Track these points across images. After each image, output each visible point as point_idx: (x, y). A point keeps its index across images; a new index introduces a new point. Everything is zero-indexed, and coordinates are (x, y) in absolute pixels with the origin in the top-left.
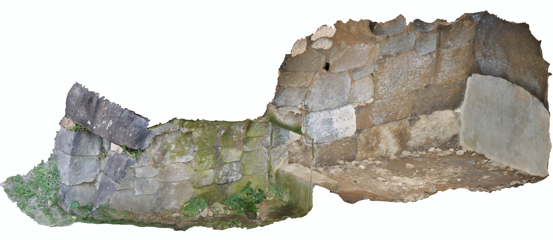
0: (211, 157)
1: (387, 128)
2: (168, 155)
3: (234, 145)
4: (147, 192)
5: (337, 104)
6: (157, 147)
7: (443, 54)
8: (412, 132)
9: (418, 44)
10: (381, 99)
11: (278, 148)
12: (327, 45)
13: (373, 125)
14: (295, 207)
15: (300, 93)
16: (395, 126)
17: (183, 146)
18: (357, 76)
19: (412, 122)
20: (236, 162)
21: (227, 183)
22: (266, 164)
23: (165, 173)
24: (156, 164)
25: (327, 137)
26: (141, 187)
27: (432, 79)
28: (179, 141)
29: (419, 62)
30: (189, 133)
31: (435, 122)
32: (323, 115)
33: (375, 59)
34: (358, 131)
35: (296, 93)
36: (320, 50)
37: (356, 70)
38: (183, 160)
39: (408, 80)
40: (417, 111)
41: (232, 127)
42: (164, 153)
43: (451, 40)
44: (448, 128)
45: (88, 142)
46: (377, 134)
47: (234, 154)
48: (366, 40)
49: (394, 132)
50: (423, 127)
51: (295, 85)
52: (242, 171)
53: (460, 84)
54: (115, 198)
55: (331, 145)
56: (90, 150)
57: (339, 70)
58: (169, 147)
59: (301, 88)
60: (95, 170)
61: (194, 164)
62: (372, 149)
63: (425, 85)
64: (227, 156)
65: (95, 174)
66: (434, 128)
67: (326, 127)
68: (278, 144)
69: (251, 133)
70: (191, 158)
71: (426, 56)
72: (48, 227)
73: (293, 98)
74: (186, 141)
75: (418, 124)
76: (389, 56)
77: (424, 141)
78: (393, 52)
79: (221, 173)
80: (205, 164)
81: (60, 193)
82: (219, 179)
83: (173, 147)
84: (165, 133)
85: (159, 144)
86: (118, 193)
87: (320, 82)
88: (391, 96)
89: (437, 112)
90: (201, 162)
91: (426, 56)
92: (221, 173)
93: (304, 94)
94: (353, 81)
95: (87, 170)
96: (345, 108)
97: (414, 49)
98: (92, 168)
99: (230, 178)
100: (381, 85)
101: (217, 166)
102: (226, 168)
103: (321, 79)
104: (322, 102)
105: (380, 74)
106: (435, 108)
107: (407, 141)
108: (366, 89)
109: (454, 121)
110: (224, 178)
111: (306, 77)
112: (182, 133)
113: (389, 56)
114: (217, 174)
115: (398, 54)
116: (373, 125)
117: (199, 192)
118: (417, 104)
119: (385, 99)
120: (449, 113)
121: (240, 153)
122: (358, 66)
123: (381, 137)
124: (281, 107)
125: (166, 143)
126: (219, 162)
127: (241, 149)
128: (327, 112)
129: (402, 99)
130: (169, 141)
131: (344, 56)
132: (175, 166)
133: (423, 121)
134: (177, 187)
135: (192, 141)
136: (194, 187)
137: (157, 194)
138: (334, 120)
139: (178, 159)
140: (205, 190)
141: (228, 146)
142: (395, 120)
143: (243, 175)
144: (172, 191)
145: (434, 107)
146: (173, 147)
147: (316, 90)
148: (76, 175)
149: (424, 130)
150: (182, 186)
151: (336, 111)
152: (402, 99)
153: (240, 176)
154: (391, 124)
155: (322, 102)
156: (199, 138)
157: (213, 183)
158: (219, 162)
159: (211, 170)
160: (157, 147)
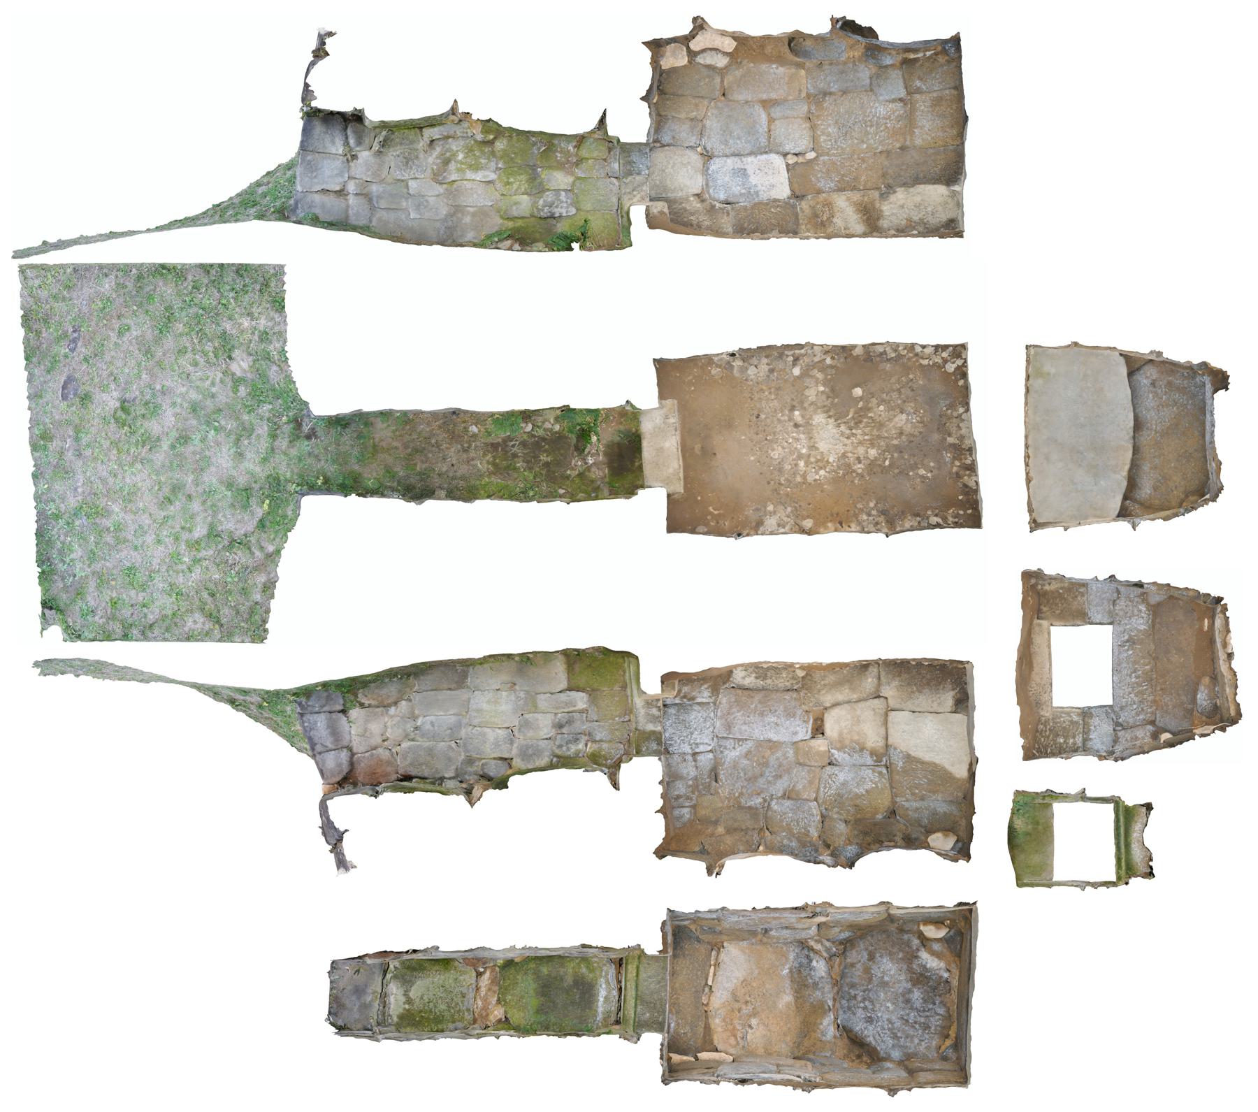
0: (523, 178)
1: (844, 198)
2: (452, 166)
3: (560, 166)
4: (427, 215)
5: (749, 148)
6: (435, 154)
7: (917, 101)
8: (884, 208)
9: (875, 83)
10: (828, 154)
11: (630, 178)
12: (721, 62)
13: (819, 192)
14: (619, 239)
15: (692, 128)
16: (856, 196)
17: (477, 158)
18: (777, 112)
19: (884, 196)
20: (565, 190)
21: (552, 217)
22: (615, 200)
23: (453, 191)
24: (438, 177)
25: (741, 194)
26: (418, 207)
27: (908, 137)
28: (471, 150)
29: (882, 110)
30: (491, 143)
31: (918, 199)
32: (731, 163)
33: (800, 91)
34: (797, 196)
35: (686, 127)
36: (710, 67)
37: (775, 103)
38: (479, 176)
39: (867, 133)
40: (891, 181)
41: (556, 142)
42: (446, 162)
43: (920, 79)
44: (940, 209)
45: (326, 133)
46: (829, 205)
47: (560, 179)
48: (780, 60)
49: (855, 204)
50: (901, 203)
51: (683, 116)
52: (576, 204)
53: (955, 150)
54: (380, 219)
55: (752, 207)
56: (328, 145)
57: (741, 97)
58: (454, 155)
59: (692, 120)
60: (341, 174)
61: (499, 185)
62: (823, 224)
63: (898, 145)
64: (549, 180)
65: (341, 180)
66: (917, 206)
67: (739, 180)
68: (630, 173)
69: (584, 152)
70: (493, 176)
71: (893, 101)
72: (877, 539)
73: (684, 135)
74: (483, 152)
75: (893, 198)
76: (831, 94)
77: (904, 222)
78: (835, 88)
79: (541, 202)
80: (515, 186)
81: (292, 202)
82: (539, 210)
83: (461, 156)
84: (448, 137)
85: (438, 149)
86: (384, 213)
87: (715, 112)
88: (843, 153)
89: (922, 186)
90: (508, 183)
91: (893, 101)
92: (541, 202)
93: (699, 129)
94: (771, 120)
95: (327, 173)
96: (765, 156)
97: (871, 90)
98: (336, 172)
99: (557, 211)
100: (823, 134)
101: (534, 191)
102: (549, 197)
103: (716, 107)
104: (726, 143)
105: (818, 117)
106: (917, 180)
107: (878, 219)
108: (797, 135)
109: (949, 200)
110: (546, 209)
111: (696, 105)
112: (476, 141)
113: (831, 94)
114: (535, 204)
115: (844, 92)
116: (819, 192)
117: (510, 224)
118: (890, 171)
119: (834, 155)
120: (941, 189)
121: (571, 179)
122: (774, 96)
123: (836, 209)
124: (668, 145)
125: (449, 150)
126: (537, 187)
127: (572, 174)
128: (736, 159)
129: (863, 160)
130: (454, 148)
131: (743, 76)
132: (468, 185)
133: (900, 195)
134: (474, 215)
135: (493, 153)
136: (502, 217)
137: (445, 220)
138: (750, 172)
139: (469, 175)
140: (520, 223)
141: (550, 167)
142: (854, 189)
143: (578, 210)
144: (468, 219)
145: (917, 178)
146: (461, 156)
147: (713, 124)
148: (311, 178)
149: (902, 207)
150: (482, 213)
151: (750, 159)
152: (863, 160)
153: (573, 211)
154: (849, 194)
155: (726, 143)
156: (504, 150)
157: (532, 216)
158: (537, 187)
159: (525, 197)
160: (435, 154)
